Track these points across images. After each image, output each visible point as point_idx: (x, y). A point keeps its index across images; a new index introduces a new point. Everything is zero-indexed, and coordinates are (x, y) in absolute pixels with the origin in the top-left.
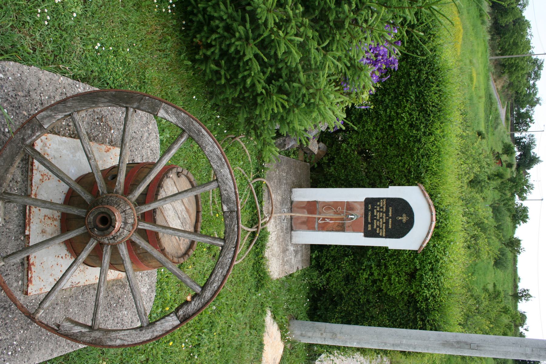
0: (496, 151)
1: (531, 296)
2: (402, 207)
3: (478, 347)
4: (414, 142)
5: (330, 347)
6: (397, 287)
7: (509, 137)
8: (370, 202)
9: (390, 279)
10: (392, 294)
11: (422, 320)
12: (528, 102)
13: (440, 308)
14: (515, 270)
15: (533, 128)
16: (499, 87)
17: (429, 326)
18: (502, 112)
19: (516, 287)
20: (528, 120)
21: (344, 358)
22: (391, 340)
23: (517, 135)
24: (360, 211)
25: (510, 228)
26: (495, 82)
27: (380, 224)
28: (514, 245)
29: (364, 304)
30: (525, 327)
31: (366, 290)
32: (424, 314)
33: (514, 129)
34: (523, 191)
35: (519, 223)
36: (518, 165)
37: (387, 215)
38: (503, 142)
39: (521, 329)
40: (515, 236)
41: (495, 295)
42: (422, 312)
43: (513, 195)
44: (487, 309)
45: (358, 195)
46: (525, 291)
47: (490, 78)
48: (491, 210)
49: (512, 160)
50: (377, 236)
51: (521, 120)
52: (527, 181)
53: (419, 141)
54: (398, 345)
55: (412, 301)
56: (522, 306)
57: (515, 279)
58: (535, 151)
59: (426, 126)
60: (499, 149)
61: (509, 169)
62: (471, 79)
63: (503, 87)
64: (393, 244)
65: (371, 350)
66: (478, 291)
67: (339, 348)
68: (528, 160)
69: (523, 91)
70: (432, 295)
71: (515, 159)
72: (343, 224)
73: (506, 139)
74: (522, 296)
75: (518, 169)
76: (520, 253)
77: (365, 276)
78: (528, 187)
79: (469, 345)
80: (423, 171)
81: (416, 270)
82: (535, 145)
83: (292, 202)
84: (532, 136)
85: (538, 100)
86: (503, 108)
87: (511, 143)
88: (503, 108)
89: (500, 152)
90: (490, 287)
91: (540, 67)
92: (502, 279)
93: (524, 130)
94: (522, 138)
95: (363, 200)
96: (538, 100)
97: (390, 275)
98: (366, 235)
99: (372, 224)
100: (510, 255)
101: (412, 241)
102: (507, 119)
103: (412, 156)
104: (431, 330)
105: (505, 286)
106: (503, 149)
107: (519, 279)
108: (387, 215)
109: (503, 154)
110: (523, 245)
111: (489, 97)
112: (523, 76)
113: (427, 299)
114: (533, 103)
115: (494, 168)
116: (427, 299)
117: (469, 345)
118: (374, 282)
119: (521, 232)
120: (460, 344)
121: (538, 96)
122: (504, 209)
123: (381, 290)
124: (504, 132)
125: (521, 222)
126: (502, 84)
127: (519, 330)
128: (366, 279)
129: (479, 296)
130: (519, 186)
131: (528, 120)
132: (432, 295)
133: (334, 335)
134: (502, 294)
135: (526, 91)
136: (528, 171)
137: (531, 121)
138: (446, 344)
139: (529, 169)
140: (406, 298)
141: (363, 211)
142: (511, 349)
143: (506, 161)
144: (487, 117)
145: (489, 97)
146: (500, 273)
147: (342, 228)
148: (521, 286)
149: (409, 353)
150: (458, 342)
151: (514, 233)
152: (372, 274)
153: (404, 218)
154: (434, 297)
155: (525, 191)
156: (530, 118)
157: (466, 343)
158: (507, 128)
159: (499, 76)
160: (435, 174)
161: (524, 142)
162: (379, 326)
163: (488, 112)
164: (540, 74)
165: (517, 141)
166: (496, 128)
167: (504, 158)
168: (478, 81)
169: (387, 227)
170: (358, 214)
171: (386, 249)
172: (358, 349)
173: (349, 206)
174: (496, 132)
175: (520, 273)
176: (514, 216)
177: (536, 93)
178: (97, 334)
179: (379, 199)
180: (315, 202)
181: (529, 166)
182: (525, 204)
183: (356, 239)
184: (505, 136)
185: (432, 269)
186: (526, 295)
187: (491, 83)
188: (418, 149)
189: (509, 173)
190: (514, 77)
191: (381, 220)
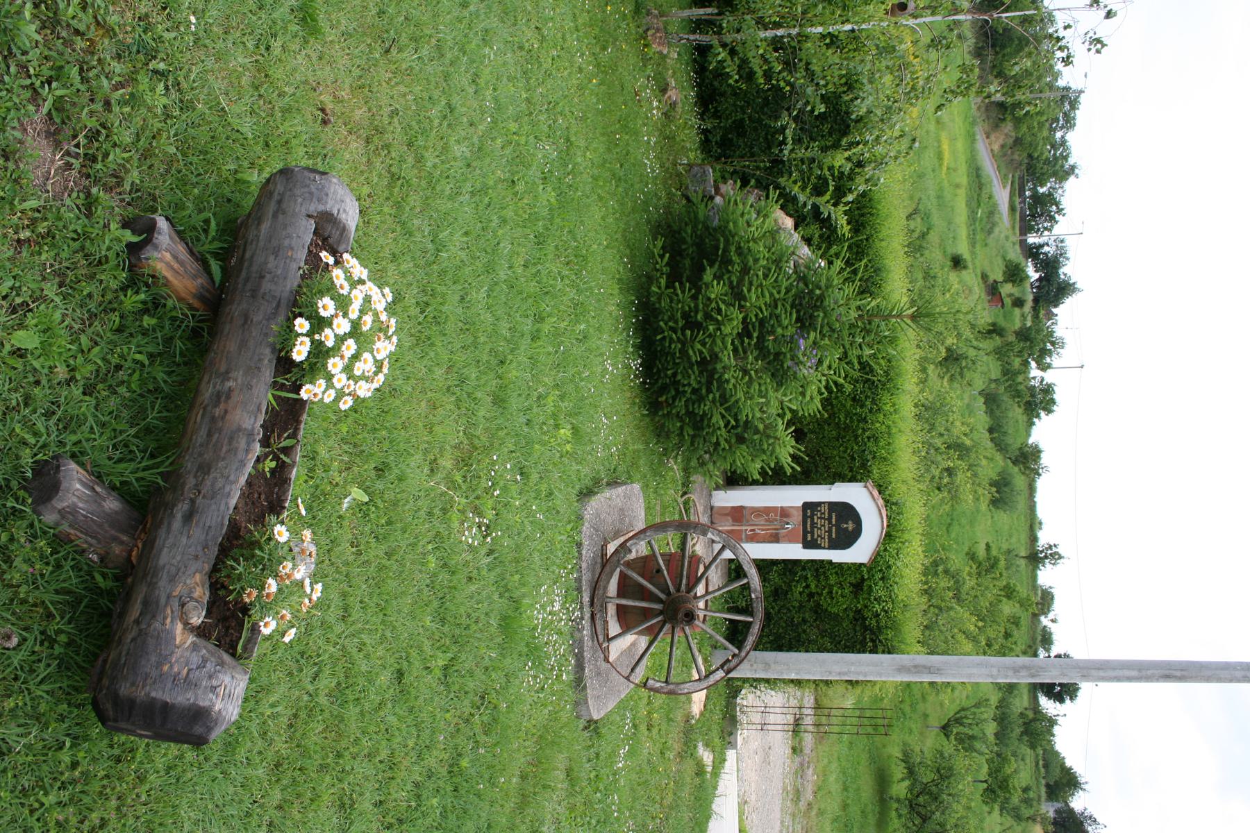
0: (992, 277)
1: (1060, 557)
2: (846, 512)
3: (938, 671)
4: (859, 421)
5: (755, 680)
6: (841, 603)
7: (1017, 247)
8: (809, 508)
9: (830, 592)
10: (834, 610)
11: (872, 640)
12: (1055, 174)
13: (895, 626)
14: (1032, 507)
15: (1062, 227)
16: (996, 147)
17: (880, 648)
18: (1002, 196)
19: (1034, 539)
20: (1054, 208)
21: (773, 693)
22: (836, 669)
23: (1032, 239)
24: (797, 518)
25: (1022, 425)
26: (988, 137)
27: (821, 532)
28: (1028, 459)
29: (799, 623)
30: (1051, 616)
31: (801, 607)
32: (874, 633)
33: (1026, 229)
34: (1044, 352)
35: (1038, 416)
36: (1036, 300)
37: (830, 522)
38: (1004, 258)
39: (1044, 621)
40: (1030, 441)
41: (987, 566)
42: (871, 630)
43: (1026, 364)
44: (973, 593)
45: (793, 497)
46: (1050, 547)
47: (978, 137)
48: (982, 400)
49: (1023, 292)
50: (818, 547)
51: (1039, 210)
52: (1051, 334)
53: (865, 420)
54: (845, 674)
55: (859, 617)
56: (1046, 576)
57: (1033, 525)
58: (1068, 270)
59: (874, 402)
60: (997, 275)
61: (1017, 311)
62: (940, 157)
63: (1002, 146)
64: (837, 556)
65: (808, 681)
66: (957, 561)
67: (767, 681)
68: (1053, 288)
69: (1042, 154)
70: (883, 610)
71: (1028, 286)
72: (777, 534)
73: (1011, 250)
74: (1046, 557)
75: (1035, 309)
76: (1039, 475)
77: (800, 589)
78: (1053, 344)
79: (929, 669)
80: (869, 457)
81: (863, 580)
82: (1068, 259)
83: (712, 508)
84: (1062, 241)
85: (1073, 168)
86: (1004, 187)
87: (1021, 259)
88: (1004, 187)
89: (1000, 278)
90: (981, 552)
91: (1074, 104)
92: (1006, 527)
93: (1046, 229)
94: (1041, 246)
95: (800, 504)
96: (1073, 168)
97: (831, 587)
98: (805, 547)
99: (812, 533)
100: (1020, 481)
101: (859, 553)
102: (1012, 208)
103: (856, 437)
104: (883, 652)
105: (1014, 540)
106: (1004, 273)
107: (1040, 523)
108: (830, 522)
109: (1006, 281)
110: (1045, 459)
111: (976, 173)
112: (1041, 125)
113: (877, 615)
114: (1064, 172)
115: (986, 316)
116: (877, 615)
117: (929, 669)
118: (811, 595)
119: (1043, 432)
120: (918, 669)
121: (1071, 161)
122: (1005, 398)
123: (818, 605)
124: (1007, 238)
125: (1042, 414)
126: (1001, 141)
127: (1039, 621)
128: (801, 593)
129: (958, 572)
130: (1037, 343)
131: (1054, 208)
132: (883, 610)
133: (767, 666)
134: (1002, 563)
135: (1047, 152)
136: (1055, 310)
137: (1059, 211)
138: (902, 669)
139: (1056, 306)
140: (851, 615)
141: (801, 518)
142: (975, 671)
143: (1010, 295)
144: (972, 218)
145: (976, 173)
146: (1003, 517)
147: (775, 539)
148: (1044, 538)
149: (857, 682)
150: (915, 667)
151: (1029, 435)
152: (807, 586)
153: (850, 526)
154: (886, 612)
155: (1050, 353)
156: (1057, 204)
157: (925, 667)
158: (1013, 228)
159: (996, 127)
160: (885, 459)
161: (1046, 254)
162: (819, 651)
163: (974, 204)
164: (1074, 119)
165: (1033, 252)
166: (990, 232)
167: (1007, 289)
168: (954, 152)
169: (830, 536)
170: (795, 523)
171: (830, 562)
172: (792, 681)
173: (784, 512)
174: (990, 241)
175: (1041, 512)
176: (1028, 404)
177: (1067, 156)
178: (672, 687)
179: (819, 504)
180: (742, 508)
181: (1056, 301)
182: (1049, 377)
183: (793, 551)
184: (1008, 245)
185: (882, 579)
186: (1054, 556)
187: (980, 137)
188: (863, 429)
189: (1018, 319)
190: (1024, 128)
191: (822, 529)
